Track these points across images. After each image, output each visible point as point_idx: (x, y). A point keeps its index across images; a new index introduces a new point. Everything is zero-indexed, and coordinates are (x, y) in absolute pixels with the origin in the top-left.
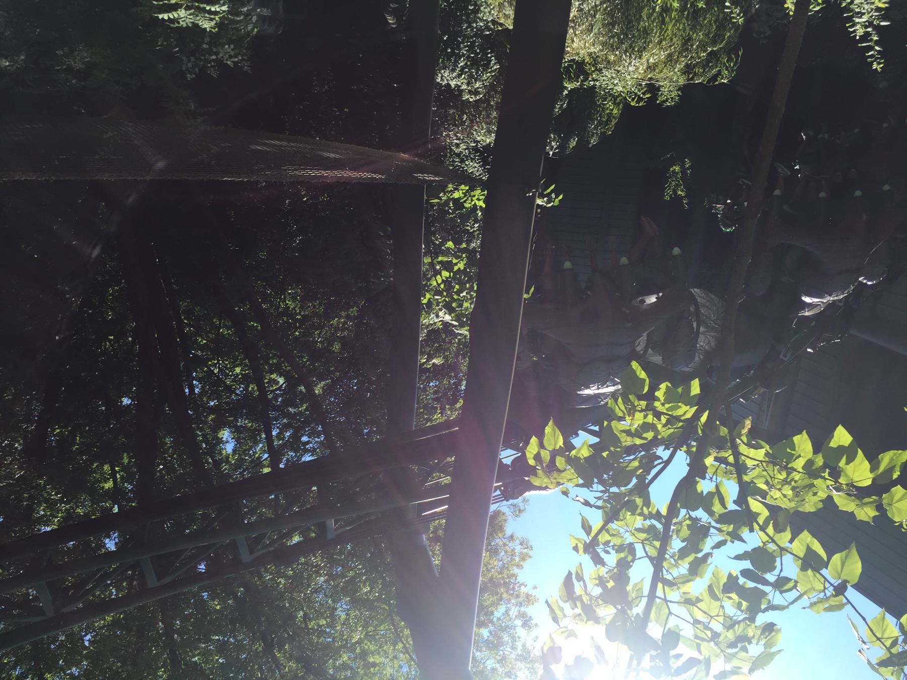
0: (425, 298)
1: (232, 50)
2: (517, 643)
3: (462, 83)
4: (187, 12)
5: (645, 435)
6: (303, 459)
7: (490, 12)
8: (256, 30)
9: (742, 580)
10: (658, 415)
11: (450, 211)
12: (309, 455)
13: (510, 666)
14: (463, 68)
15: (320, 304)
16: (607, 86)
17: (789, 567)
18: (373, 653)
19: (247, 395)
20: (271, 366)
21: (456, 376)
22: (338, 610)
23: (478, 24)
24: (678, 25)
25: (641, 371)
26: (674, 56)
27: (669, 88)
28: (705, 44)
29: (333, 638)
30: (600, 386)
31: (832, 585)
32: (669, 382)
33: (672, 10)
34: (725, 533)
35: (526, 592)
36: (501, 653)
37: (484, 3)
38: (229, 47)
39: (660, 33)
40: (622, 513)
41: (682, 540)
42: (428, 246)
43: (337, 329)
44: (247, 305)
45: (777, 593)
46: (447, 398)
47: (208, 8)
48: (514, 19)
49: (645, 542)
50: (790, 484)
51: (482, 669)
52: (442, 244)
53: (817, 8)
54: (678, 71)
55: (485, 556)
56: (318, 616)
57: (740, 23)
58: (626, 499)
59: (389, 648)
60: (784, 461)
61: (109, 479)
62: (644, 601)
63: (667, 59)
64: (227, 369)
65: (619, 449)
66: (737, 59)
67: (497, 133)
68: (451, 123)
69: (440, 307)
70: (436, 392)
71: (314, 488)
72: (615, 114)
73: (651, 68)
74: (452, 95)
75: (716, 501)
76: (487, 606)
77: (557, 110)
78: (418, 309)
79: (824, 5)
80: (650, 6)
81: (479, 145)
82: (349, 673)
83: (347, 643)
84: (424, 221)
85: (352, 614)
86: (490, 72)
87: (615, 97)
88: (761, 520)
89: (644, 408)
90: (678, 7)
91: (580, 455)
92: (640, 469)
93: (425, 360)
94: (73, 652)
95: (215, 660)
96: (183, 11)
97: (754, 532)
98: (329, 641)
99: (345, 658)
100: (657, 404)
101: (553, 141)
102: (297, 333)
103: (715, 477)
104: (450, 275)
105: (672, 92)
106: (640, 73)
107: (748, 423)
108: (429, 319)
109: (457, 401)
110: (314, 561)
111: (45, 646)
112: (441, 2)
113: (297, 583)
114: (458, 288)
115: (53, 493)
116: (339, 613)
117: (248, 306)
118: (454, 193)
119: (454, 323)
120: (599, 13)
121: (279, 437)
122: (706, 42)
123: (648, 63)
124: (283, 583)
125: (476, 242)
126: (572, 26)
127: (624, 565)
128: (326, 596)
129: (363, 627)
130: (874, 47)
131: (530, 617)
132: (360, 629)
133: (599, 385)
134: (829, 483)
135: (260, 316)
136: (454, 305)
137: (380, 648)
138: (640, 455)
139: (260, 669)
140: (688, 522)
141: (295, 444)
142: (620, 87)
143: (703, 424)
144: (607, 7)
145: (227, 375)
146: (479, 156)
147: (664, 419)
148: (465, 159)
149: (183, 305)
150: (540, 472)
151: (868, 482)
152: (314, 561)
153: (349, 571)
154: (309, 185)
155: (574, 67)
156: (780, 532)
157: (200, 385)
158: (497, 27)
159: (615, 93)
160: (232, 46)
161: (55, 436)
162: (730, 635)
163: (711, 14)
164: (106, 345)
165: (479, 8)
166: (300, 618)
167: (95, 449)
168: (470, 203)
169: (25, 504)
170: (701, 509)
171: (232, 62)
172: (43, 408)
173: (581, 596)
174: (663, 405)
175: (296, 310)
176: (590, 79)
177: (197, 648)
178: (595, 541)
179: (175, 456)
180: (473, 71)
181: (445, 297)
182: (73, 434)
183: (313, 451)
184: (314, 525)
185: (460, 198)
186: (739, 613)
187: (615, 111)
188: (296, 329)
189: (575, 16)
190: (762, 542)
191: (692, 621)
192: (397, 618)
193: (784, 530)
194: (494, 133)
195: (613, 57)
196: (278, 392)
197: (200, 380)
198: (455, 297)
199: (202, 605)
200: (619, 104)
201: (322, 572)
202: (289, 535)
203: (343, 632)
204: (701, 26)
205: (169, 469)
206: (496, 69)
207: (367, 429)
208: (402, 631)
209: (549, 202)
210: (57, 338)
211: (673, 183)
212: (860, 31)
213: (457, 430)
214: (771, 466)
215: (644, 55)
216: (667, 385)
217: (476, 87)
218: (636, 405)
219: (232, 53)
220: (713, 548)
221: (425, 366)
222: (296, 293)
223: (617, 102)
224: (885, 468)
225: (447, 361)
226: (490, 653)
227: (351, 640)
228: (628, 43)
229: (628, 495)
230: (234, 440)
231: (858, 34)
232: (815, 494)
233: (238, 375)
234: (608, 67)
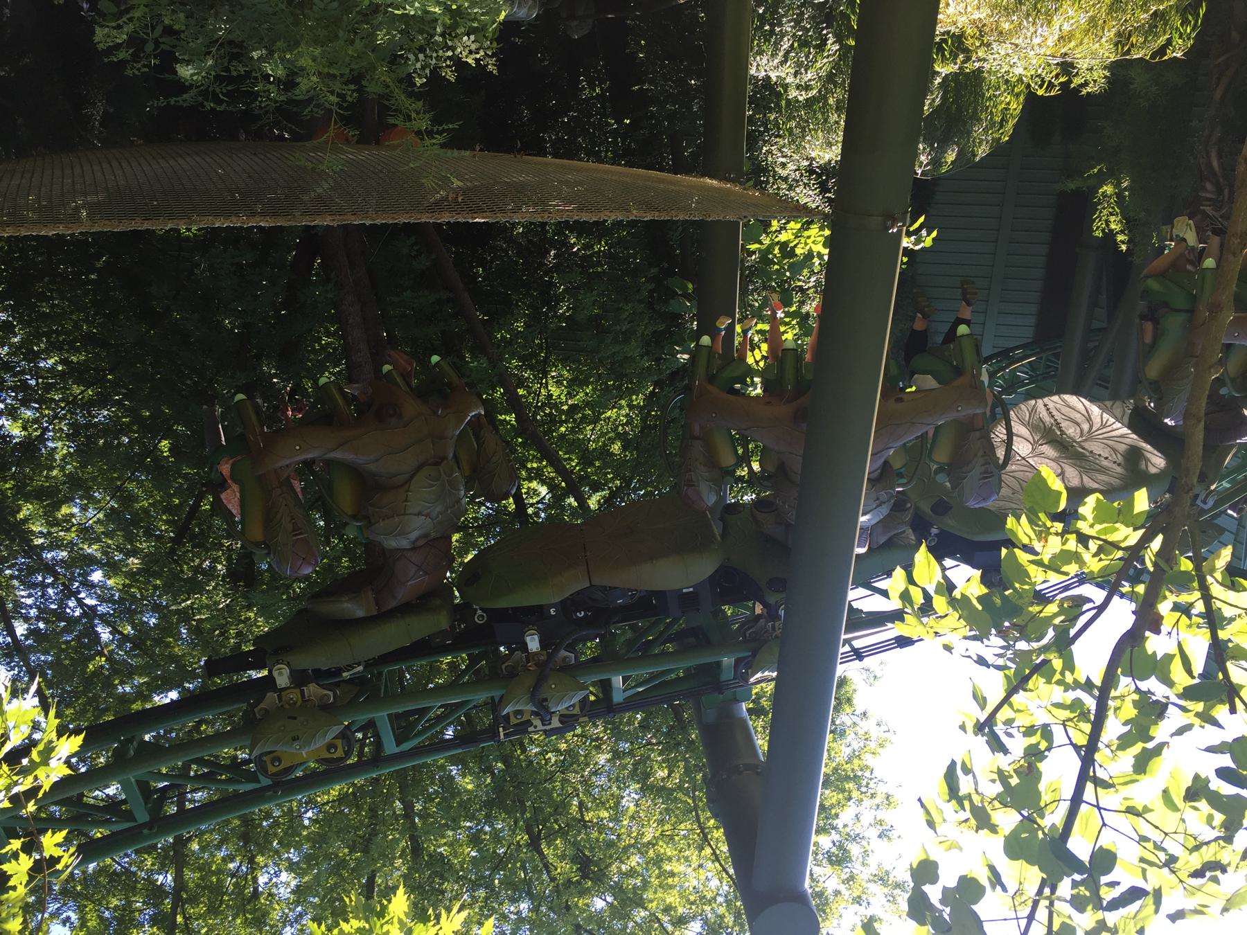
5: (1064, 569)
10: (1083, 539)
13: (861, 889)
14: (787, 53)
18: (670, 859)
20: (529, 470)
29: (619, 835)
59: (692, 854)
72: (1015, 109)
74: (770, 92)
81: (815, 164)
82: (638, 882)
113: (571, 760)
123: (1061, 30)
127: (1034, 755)
140: (1136, 697)
147: (1093, 545)
160: (472, 38)
162: (1196, 861)
174: (1092, 526)
176: (974, 59)
178: (991, 719)
187: (1013, 106)
188: (561, 423)
191: (1137, 839)
196: (540, 506)
200: (1018, 95)
209: (917, 242)
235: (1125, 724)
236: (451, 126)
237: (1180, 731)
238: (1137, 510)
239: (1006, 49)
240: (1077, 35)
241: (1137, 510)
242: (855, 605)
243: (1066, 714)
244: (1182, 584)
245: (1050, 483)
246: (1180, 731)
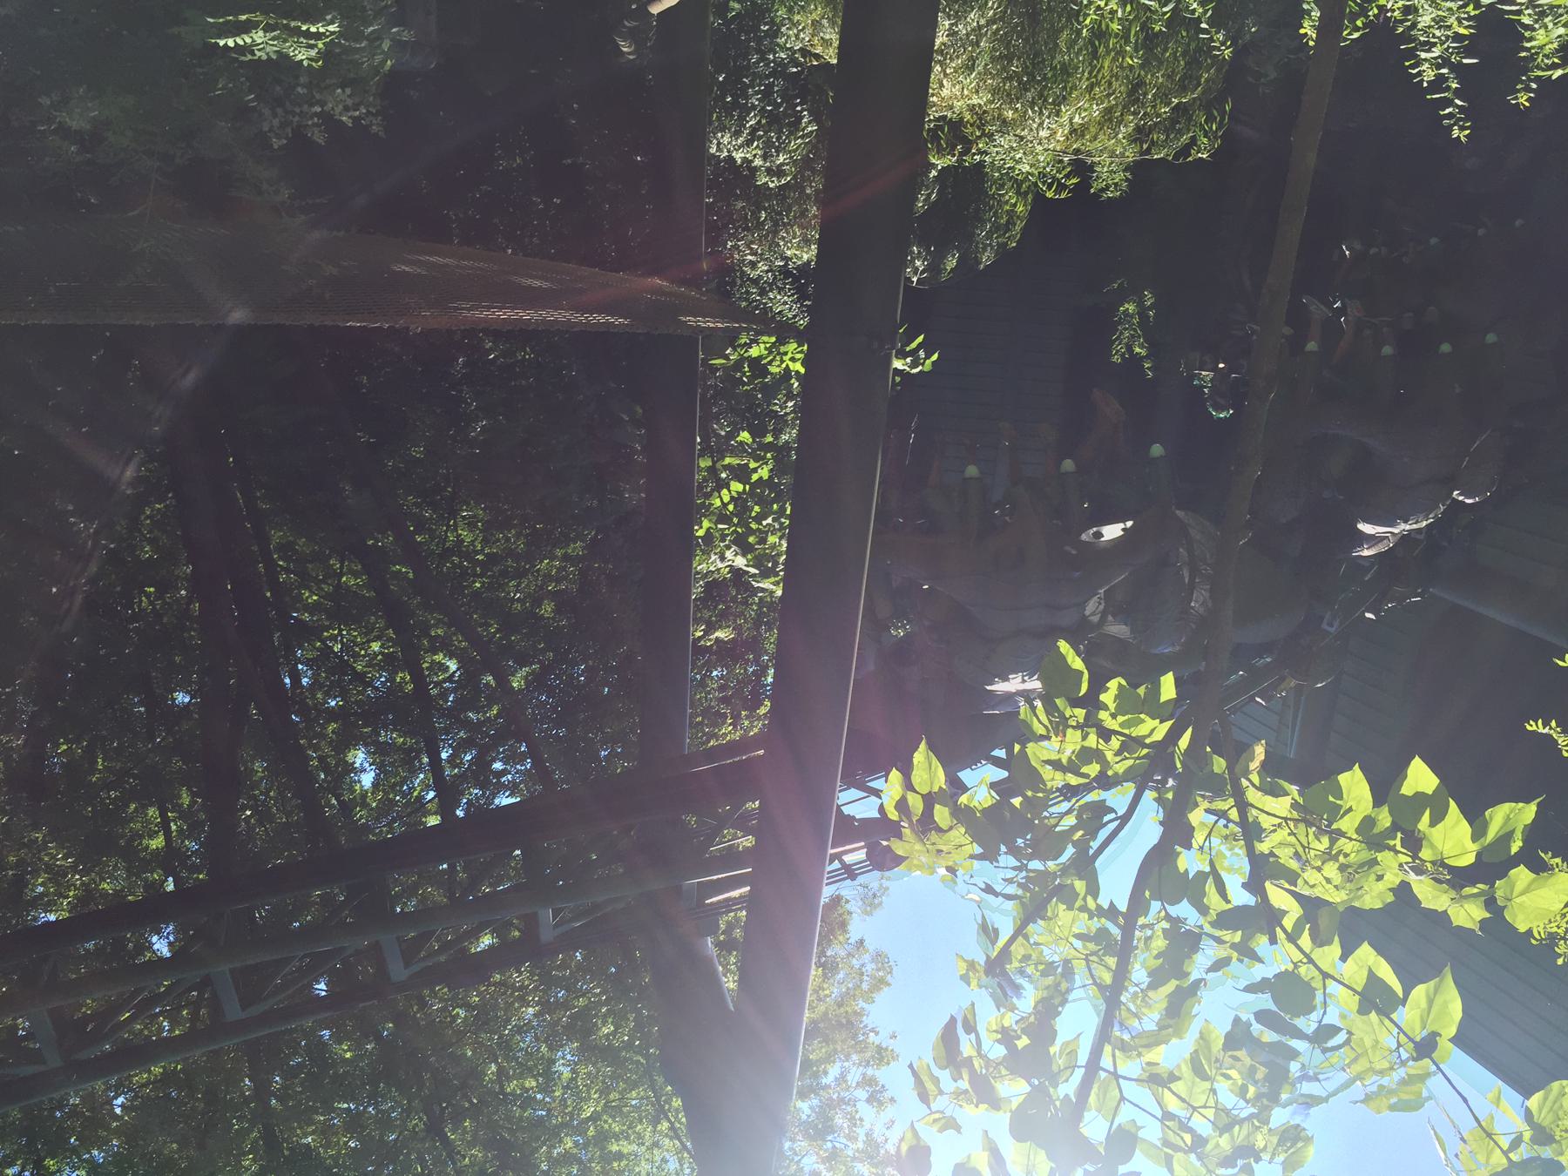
0: (701, 527)
1: (349, 96)
2: (858, 1130)
3: (755, 156)
4: (268, 34)
5: (1084, 770)
6: (497, 801)
7: (797, 36)
8: (389, 62)
9: (1256, 1028)
10: (1106, 734)
11: (744, 379)
12: (507, 794)
14: (754, 130)
15: (518, 536)
16: (1005, 164)
17: (1340, 1005)
18: (617, 1137)
19: (394, 689)
20: (433, 639)
21: (757, 661)
22: (557, 1064)
23: (777, 55)
24: (1120, 60)
25: (1074, 657)
26: (1115, 112)
27: (1110, 166)
28: (1167, 92)
29: (549, 1111)
30: (1026, 678)
31: (1411, 1040)
32: (1123, 677)
33: (1110, 35)
34: (1229, 944)
35: (877, 1043)
36: (829, 1145)
37: (787, 21)
38: (344, 91)
39: (1090, 73)
40: (1051, 906)
42: (705, 439)
43: (548, 577)
44: (389, 536)
45: (1318, 1052)
46: (745, 697)
47: (304, 28)
48: (839, 48)
49: (1091, 958)
50: (1337, 860)
51: (795, 1172)
52: (732, 435)
53: (1356, 35)
54: (1124, 138)
55: (816, 976)
57: (1226, 57)
58: (1056, 883)
60: (1325, 817)
61: (157, 832)
62: (1079, 1074)
63: (1103, 117)
64: (356, 644)
65: (1041, 795)
66: (1222, 119)
67: (820, 243)
68: (740, 226)
69: (727, 543)
70: (722, 688)
71: (518, 852)
73: (1076, 132)
75: (1210, 888)
77: (920, 205)
78: (687, 547)
79: (1367, 30)
80: (1071, 29)
83: (572, 1119)
84: (699, 395)
85: (583, 1070)
86: (802, 137)
87: (1019, 184)
88: (1288, 923)
89: (1081, 721)
90: (1119, 30)
91: (975, 803)
92: (1077, 831)
93: (702, 633)
94: (94, 1123)
95: (341, 1143)
96: (261, 33)
97: (1276, 943)
98: (542, 1115)
99: (569, 1143)
100: (1103, 715)
101: (918, 259)
102: (478, 585)
105: (1115, 173)
106: (1058, 141)
107: (1260, 751)
108: (707, 564)
109: (760, 704)
110: (518, 979)
111: (46, 1113)
112: (712, 19)
113: (484, 1018)
114: (759, 510)
115: (60, 856)
117: (391, 538)
118: (751, 347)
119: (753, 571)
121: (451, 760)
122: (1170, 89)
123: (1071, 123)
124: (463, 1016)
125: (790, 433)
126: (940, 61)
130: (1453, 100)
131: (883, 1086)
133: (1026, 676)
134: (1403, 859)
135: (413, 554)
136: (751, 539)
137: (629, 1128)
138: (1077, 805)
139: (422, 1161)
140: (1166, 925)
141: (481, 774)
142: (1026, 165)
143: (1183, 751)
144: (998, 30)
145: (356, 656)
146: (791, 284)
147: (1115, 743)
148: (768, 289)
149: (276, 536)
150: (907, 832)
151: (1469, 859)
152: (518, 979)
153: (577, 998)
154: (500, 333)
155: (946, 129)
156: (1321, 945)
157: (310, 673)
158: (811, 61)
159: (1018, 175)
160: (348, 91)
163: (1176, 41)
164: (141, 601)
166: (491, 1076)
167: (132, 781)
168: (779, 366)
169: (11, 873)
171: (349, 117)
172: (36, 709)
174: (1114, 716)
175: (474, 546)
176: (973, 151)
177: (311, 1122)
179: (272, 794)
180: (772, 134)
183: (513, 788)
185: (760, 358)
186: (1242, 1103)
187: (1020, 208)
189: (944, 44)
190: (1292, 961)
191: (1159, 1114)
192: (660, 1080)
193: (1329, 942)
194: (814, 244)
195: (1010, 112)
197: (307, 662)
198: (754, 526)
199: (319, 1051)
200: (1026, 193)
201: (531, 998)
202: (475, 935)
203: (565, 1100)
204: (1161, 63)
205: (263, 815)
206: (812, 132)
207: (605, 750)
208: (668, 1101)
209: (914, 365)
210: (54, 590)
211: (1127, 334)
212: (1429, 75)
213: (759, 756)
214: (1302, 826)
216: (1119, 683)
217: (778, 162)
218: (1068, 716)
219: (349, 102)
220: (1209, 970)
221: (702, 643)
222: (474, 516)
223: (1022, 190)
224: (1496, 836)
225: (739, 634)
226: (809, 1145)
227: (579, 1115)
228: (1035, 89)
229: (1060, 876)
230: (373, 767)
231: (1425, 79)
232: (1380, 878)
233: (375, 655)
235: (1157, 957)
236: (318, 201)
237: (1219, 965)
238: (1164, 698)
239: (1010, 141)
240: (1092, 129)
241: (1164, 698)
242: (846, 810)
243: (1092, 946)
244: (1216, 787)
245: (1069, 660)
246: (1219, 965)
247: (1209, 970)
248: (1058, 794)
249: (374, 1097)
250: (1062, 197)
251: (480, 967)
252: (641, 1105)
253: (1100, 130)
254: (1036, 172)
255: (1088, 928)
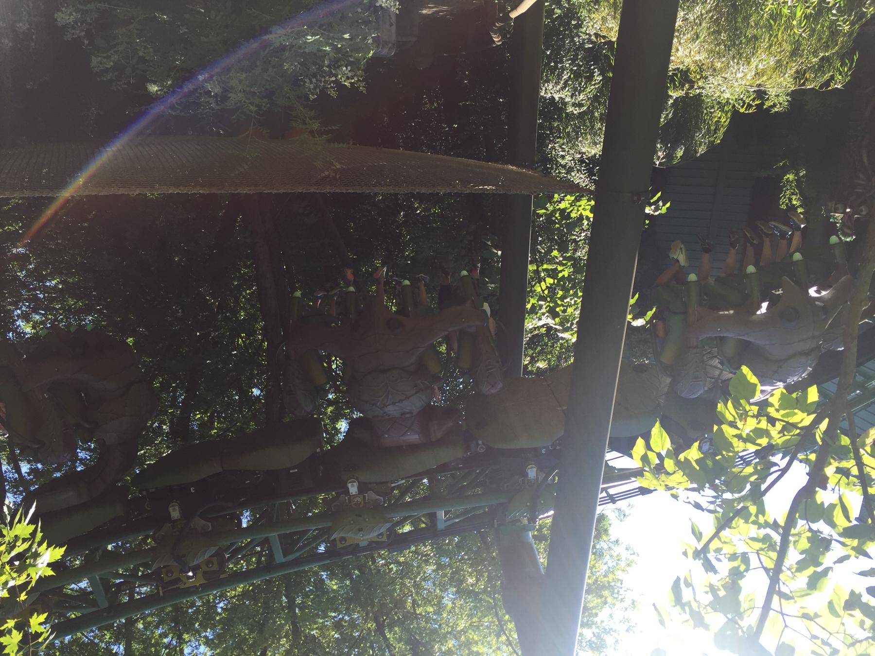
1: (349, 71)
5: (758, 441)
7: (593, 26)
10: (772, 421)
18: (476, 643)
29: (440, 625)
37: (588, 18)
38: (347, 69)
41: (800, 551)
49: (760, 552)
54: (789, 77)
56: (425, 603)
59: (493, 639)
62: (758, 612)
65: (731, 454)
66: (851, 64)
74: (555, 108)
76: (591, 608)
78: (521, 314)
81: (585, 157)
93: (528, 362)
103: (837, 488)
104: (554, 282)
113: (406, 570)
116: (446, 602)
120: (704, 21)
126: (677, 36)
127: (736, 575)
128: (434, 585)
129: (468, 617)
132: (465, 618)
139: (372, 647)
140: (809, 534)
144: (713, 16)
147: (779, 426)
160: (349, 68)
161: (197, 420)
164: (238, 341)
165: (582, 23)
170: (822, 521)
171: (349, 83)
173: (690, 602)
176: (696, 87)
178: (706, 548)
181: (549, 302)
182: (211, 420)
184: (424, 516)
187: (723, 120)
189: (680, 26)
191: (809, 636)
195: (719, 63)
200: (727, 112)
202: (401, 523)
208: (506, 623)
210: (198, 334)
215: (753, 61)
216: (782, 392)
218: (748, 410)
219: (350, 74)
220: (835, 563)
227: (456, 628)
234: (715, 74)
237: (841, 560)
238: (810, 400)
240: (769, 72)
241: (810, 400)
242: (610, 463)
243: (759, 545)
244: (842, 453)
245: (749, 378)
246: (841, 560)
247: (835, 563)
248: (740, 459)
249: (348, 612)
250: (750, 112)
251: (402, 541)
252: (490, 626)
253: (774, 72)
254: (734, 98)
255: (757, 534)
